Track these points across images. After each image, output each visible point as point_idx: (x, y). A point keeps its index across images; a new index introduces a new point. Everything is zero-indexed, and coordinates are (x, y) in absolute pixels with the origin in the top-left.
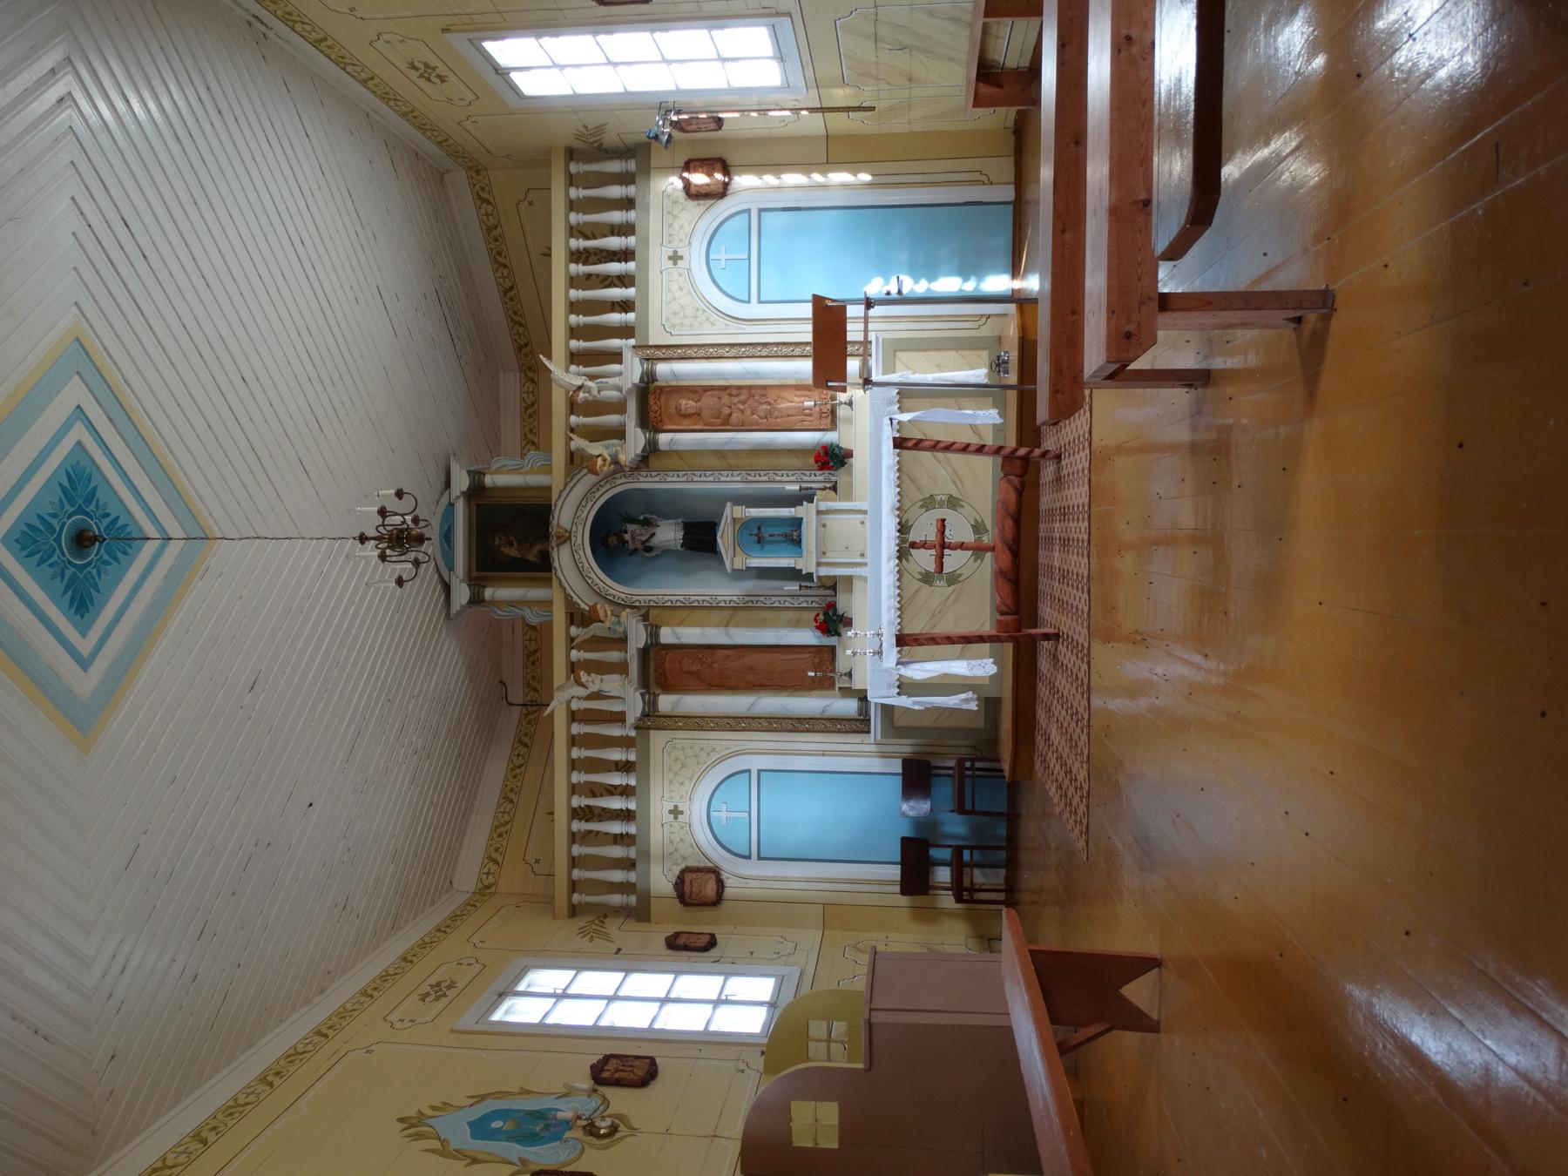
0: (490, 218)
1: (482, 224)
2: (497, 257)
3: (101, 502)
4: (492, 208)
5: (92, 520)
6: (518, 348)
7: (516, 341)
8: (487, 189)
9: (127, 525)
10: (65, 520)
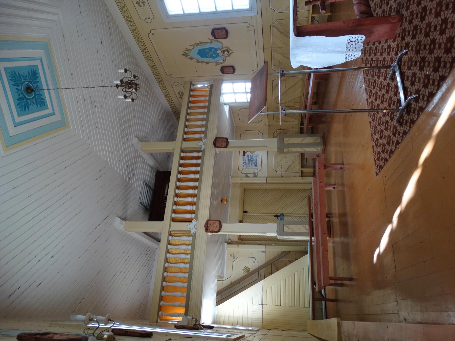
0: (133, 26)
1: (150, 66)
2: (138, 39)
3: (18, 94)
4: (143, 44)
5: (23, 92)
6: (132, 31)
7: (141, 48)
8: (140, 38)
9: (10, 79)
10: (31, 99)
